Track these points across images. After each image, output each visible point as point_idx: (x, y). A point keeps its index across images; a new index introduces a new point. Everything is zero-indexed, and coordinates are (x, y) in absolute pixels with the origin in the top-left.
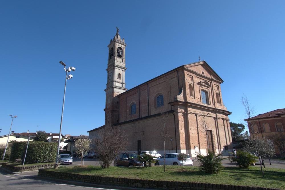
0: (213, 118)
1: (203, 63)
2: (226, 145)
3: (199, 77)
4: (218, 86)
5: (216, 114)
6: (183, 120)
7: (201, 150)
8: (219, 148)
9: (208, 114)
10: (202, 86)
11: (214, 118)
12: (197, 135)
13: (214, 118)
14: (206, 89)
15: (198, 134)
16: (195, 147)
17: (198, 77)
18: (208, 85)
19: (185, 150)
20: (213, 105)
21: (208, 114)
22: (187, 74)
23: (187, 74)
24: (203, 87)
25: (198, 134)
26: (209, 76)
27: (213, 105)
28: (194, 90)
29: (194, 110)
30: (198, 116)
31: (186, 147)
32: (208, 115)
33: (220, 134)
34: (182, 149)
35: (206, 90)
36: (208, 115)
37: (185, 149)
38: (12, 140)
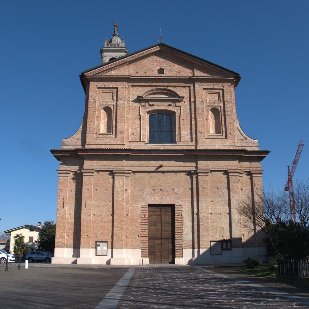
0: (183, 174)
1: (158, 48)
2: (227, 237)
3: (138, 84)
4: (223, 90)
5: (197, 164)
6: (75, 188)
7: (114, 250)
8: (195, 243)
9: (161, 166)
10: (150, 103)
11: (189, 173)
12: (111, 217)
13: (189, 173)
14: (170, 106)
15: (113, 215)
16: (98, 243)
17: (139, 86)
18: (175, 97)
19: (73, 249)
20: (192, 141)
21: (161, 166)
22: (99, 88)
23: (99, 88)
24: (155, 103)
25: (113, 215)
26: (186, 73)
27: (192, 141)
28: (116, 118)
29: (105, 162)
30: (230, 174)
31: (74, 243)
32: (161, 169)
33: (200, 211)
34: (58, 247)
35: (170, 109)
36: (161, 169)
37: (71, 248)
38: (48, 221)
